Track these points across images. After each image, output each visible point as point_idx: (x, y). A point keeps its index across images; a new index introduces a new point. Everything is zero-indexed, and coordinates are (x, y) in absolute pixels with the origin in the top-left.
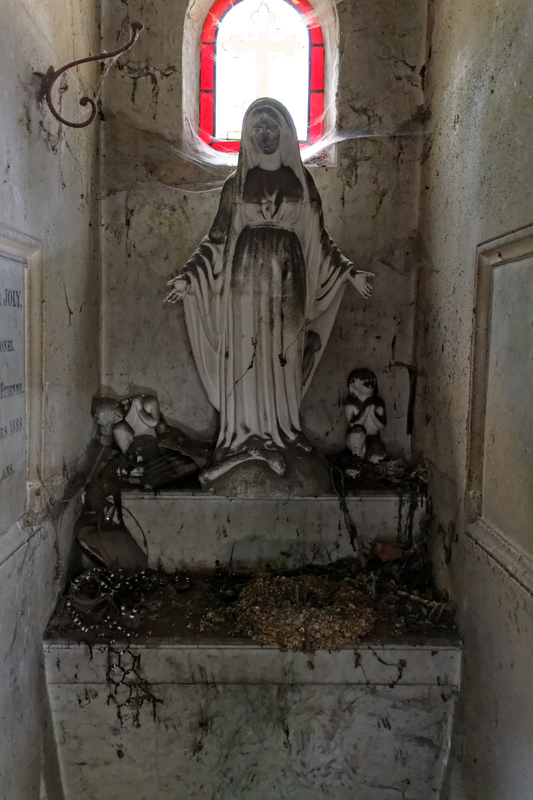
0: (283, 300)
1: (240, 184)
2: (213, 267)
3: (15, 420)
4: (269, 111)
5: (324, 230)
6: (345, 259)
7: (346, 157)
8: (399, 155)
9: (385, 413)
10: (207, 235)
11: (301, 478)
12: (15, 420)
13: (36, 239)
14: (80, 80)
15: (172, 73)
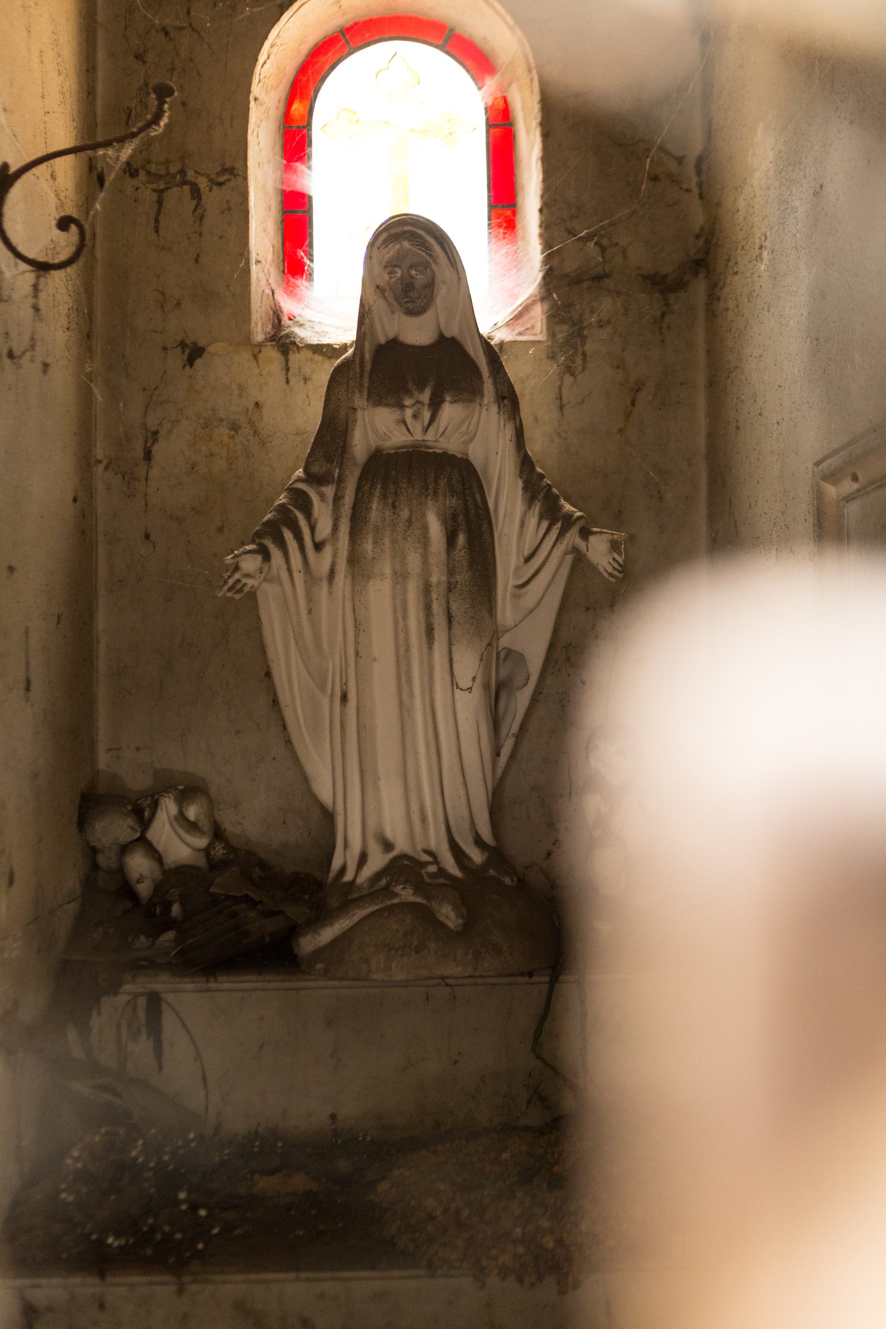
0: (450, 588)
1: (362, 371)
2: (312, 529)
4: (413, 237)
6: (568, 507)
7: (563, 321)
8: (663, 315)
10: (301, 470)
14: (57, 195)
15: (229, 180)
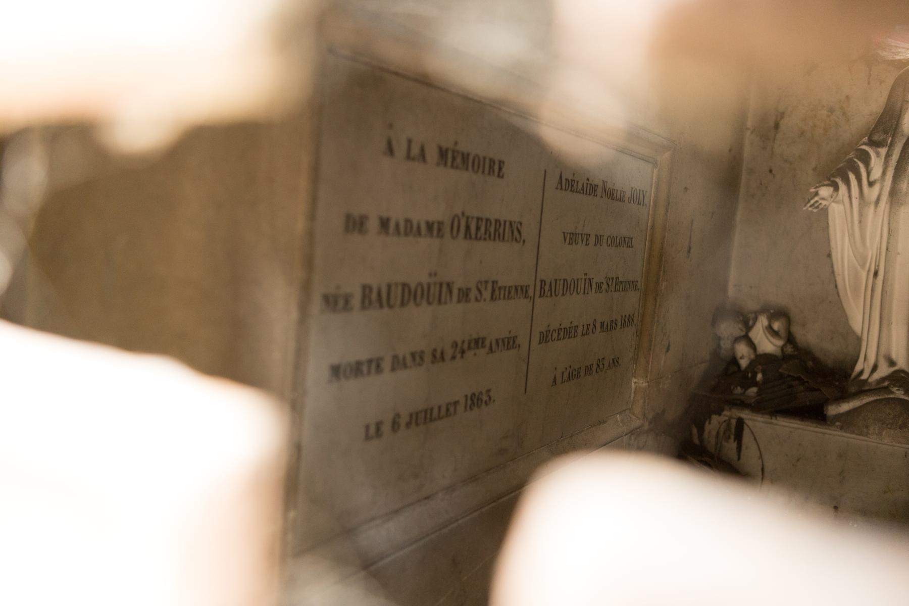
2: (868, 174)
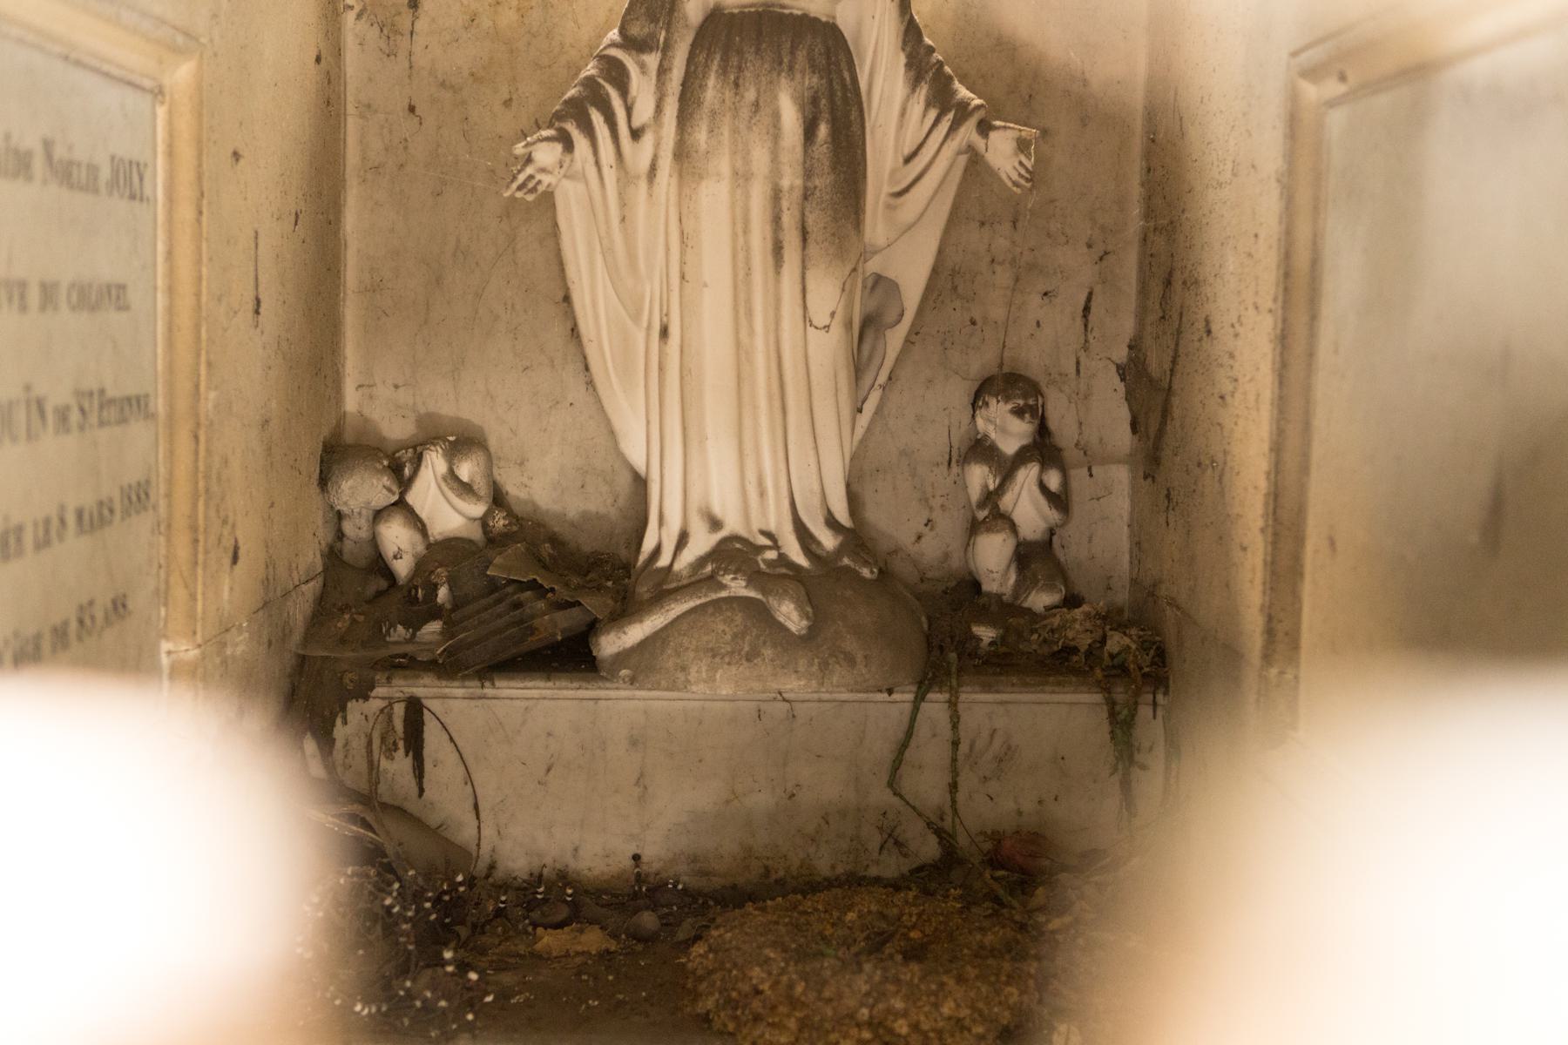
2: (629, 111)
3: (134, 484)
5: (912, 20)
6: (963, 92)
9: (1065, 483)
10: (616, 31)
11: (850, 644)
12: (134, 484)
13: (187, 34)
